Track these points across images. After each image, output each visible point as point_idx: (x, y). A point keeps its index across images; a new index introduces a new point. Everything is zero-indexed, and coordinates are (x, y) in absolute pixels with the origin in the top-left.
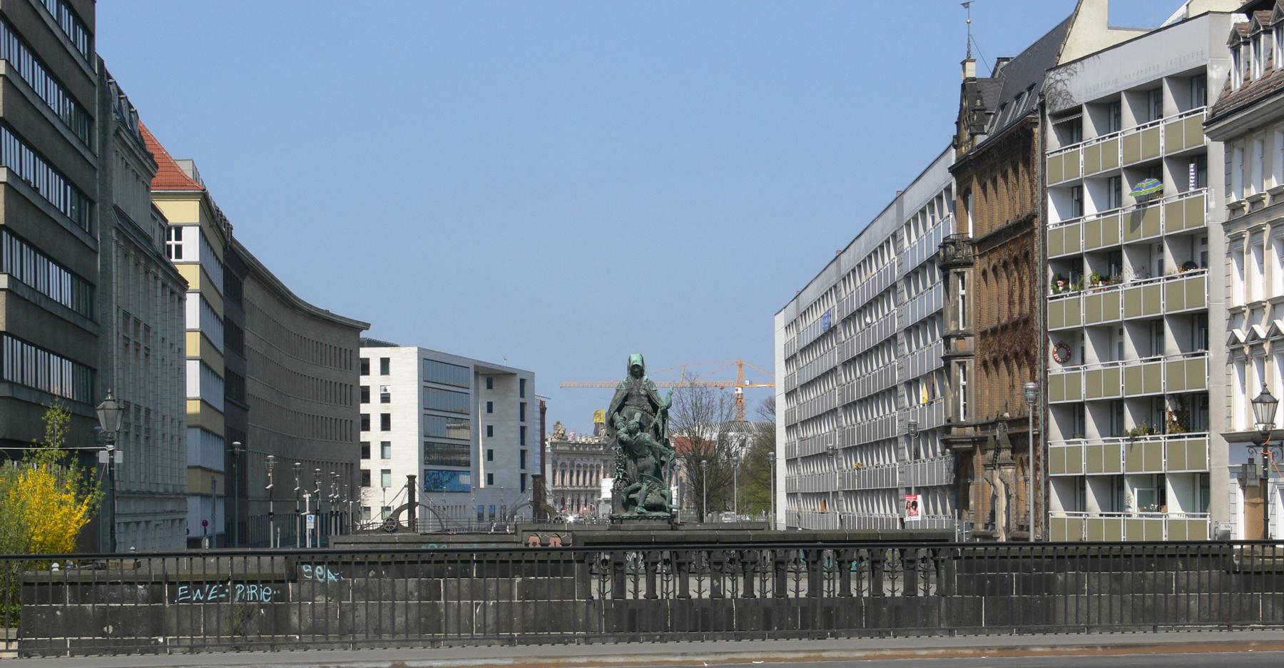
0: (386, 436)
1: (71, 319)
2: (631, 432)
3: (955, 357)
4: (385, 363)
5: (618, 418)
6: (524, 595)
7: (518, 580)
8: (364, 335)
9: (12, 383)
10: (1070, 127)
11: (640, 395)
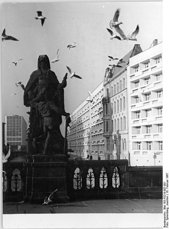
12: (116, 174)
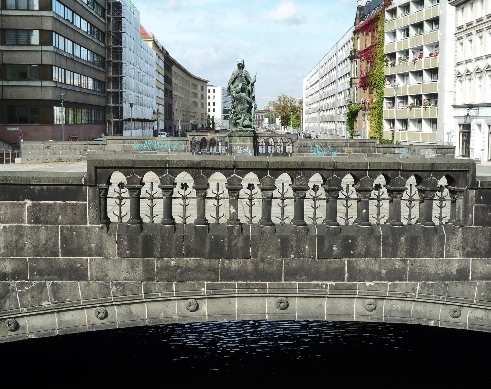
1: (89, 64)
2: (237, 93)
3: (354, 84)
4: (214, 91)
5: (232, 86)
6: (36, 219)
7: (29, 203)
8: (208, 84)
9: (56, 82)
10: (393, 12)
11: (242, 77)
12: (411, 192)
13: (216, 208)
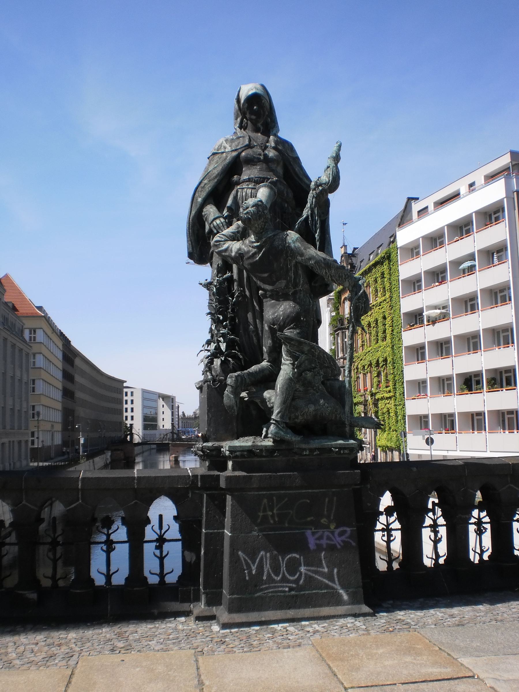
0: (132, 414)
4: (132, 393)
13: (432, 543)
